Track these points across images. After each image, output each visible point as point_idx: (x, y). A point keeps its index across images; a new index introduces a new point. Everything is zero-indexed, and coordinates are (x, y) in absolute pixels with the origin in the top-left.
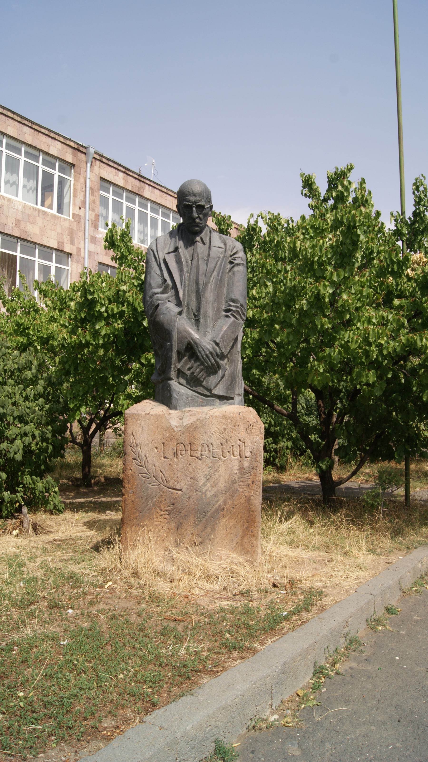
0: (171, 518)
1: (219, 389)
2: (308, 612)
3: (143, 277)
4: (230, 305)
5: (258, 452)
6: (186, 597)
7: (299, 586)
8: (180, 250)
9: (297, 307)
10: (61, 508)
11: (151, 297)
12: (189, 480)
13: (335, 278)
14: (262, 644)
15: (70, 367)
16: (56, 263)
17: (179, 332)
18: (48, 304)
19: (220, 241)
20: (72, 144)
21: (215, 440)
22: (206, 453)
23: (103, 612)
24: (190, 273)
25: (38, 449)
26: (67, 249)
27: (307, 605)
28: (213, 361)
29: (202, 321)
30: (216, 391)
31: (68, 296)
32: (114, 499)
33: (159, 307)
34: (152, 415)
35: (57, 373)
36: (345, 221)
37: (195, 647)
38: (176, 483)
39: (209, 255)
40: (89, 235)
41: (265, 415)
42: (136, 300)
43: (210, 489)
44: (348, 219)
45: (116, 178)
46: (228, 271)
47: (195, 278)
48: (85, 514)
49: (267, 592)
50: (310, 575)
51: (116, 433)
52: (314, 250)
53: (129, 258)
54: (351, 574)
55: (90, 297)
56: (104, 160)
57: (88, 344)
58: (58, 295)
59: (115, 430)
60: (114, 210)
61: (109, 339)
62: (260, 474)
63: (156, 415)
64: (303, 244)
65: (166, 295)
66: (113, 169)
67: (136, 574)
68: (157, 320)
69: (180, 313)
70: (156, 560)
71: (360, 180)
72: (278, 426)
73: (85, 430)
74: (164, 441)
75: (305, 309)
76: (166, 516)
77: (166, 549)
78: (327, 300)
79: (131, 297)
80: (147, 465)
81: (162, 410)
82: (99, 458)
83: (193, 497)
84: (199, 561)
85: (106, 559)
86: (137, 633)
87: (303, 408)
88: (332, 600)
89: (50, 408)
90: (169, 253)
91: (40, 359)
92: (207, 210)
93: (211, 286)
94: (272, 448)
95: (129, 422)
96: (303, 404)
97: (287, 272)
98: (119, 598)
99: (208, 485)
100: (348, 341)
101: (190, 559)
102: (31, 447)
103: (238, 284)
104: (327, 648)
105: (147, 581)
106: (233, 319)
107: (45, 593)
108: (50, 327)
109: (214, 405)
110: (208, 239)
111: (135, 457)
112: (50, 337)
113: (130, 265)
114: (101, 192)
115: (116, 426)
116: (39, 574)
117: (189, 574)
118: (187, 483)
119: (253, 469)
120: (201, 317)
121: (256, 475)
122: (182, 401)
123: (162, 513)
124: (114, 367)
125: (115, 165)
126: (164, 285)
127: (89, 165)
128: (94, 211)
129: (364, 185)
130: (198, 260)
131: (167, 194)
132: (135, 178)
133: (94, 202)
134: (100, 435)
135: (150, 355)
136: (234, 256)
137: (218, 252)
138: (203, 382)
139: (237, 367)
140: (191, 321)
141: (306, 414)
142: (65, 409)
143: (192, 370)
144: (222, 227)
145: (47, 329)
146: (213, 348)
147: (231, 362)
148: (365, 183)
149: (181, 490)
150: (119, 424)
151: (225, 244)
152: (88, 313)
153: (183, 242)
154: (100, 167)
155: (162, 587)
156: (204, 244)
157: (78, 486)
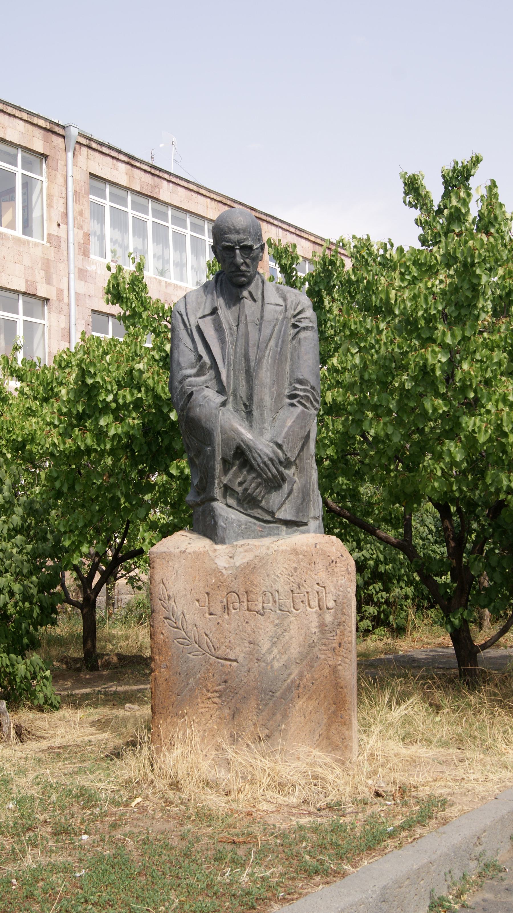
0: (223, 702)
1: (285, 510)
2: (424, 826)
3: (168, 347)
4: (296, 389)
5: (345, 601)
6: (249, 814)
7: (414, 794)
8: (219, 311)
9: (397, 385)
10: (55, 703)
11: (181, 382)
12: (247, 645)
13: (448, 340)
14: (354, 866)
15: (62, 485)
16: (24, 314)
17: (223, 432)
18: (25, 391)
19: (277, 295)
20: (42, 123)
21: (282, 586)
22: (270, 605)
23: (131, 835)
24: (236, 345)
25: (18, 612)
26: (41, 292)
27: (424, 818)
28: (274, 470)
29: (255, 413)
30: (281, 515)
31: (56, 379)
32: (135, 687)
33: (194, 397)
34: (190, 554)
35: (44, 496)
36: (459, 255)
37: (260, 872)
38: (228, 650)
39: (262, 317)
40: (75, 267)
41: (369, 546)
42: (158, 382)
43: (278, 657)
44: (463, 253)
45: (115, 172)
46: (290, 338)
47: (243, 352)
48: (92, 710)
49: (366, 804)
50: (431, 779)
51: (132, 584)
52: (416, 302)
53: (144, 315)
54: (491, 776)
55: (90, 381)
56: (94, 145)
57: (89, 451)
58: (41, 379)
59: (131, 580)
60: (113, 225)
61: (119, 442)
62: (350, 632)
63: (195, 552)
64: (399, 294)
65: (202, 379)
66: (108, 159)
67: (175, 786)
68: (191, 414)
69: (224, 404)
70: (205, 765)
71: (489, 183)
72: (391, 562)
73: (85, 582)
74: (208, 590)
75: (406, 387)
76: (216, 700)
77: (219, 748)
78: (438, 373)
79: (151, 380)
80: (185, 627)
81: (203, 545)
82: (107, 627)
83: (253, 670)
84: (267, 763)
85: (131, 767)
86: (181, 859)
87: (430, 531)
88: (459, 810)
89: (33, 549)
90: (204, 317)
91: (14, 476)
92: (257, 251)
93: (267, 363)
94: (382, 598)
95: (156, 565)
96: (430, 526)
97: (380, 332)
98: (153, 818)
99: (275, 651)
100: (473, 431)
101: (253, 761)
102: (7, 610)
103: (306, 357)
104: (450, 872)
105: (192, 794)
106: (300, 408)
107: (46, 816)
108: (27, 424)
109: (279, 534)
110: (260, 292)
111: (167, 616)
112: (27, 441)
113: (147, 326)
114: (91, 196)
115: (132, 574)
116: (35, 792)
117: (252, 782)
118: (245, 650)
119: (339, 625)
120: (254, 407)
121: (343, 635)
122: (232, 531)
123: (210, 695)
124: (128, 481)
125: (112, 153)
126: (199, 364)
127: (70, 154)
128: (81, 227)
129: (494, 191)
130: (246, 325)
131: (199, 193)
132: (145, 171)
133: (81, 213)
134: (108, 589)
135: (183, 463)
136: (299, 317)
137: (276, 311)
138: (261, 501)
139: (310, 478)
140: (240, 415)
141: (436, 542)
142: (57, 551)
143: (244, 486)
144: (284, 261)
145: (22, 428)
146: (274, 452)
147: (301, 470)
148: (495, 186)
149: (235, 661)
150: (137, 570)
151: (285, 300)
152: (88, 404)
153: (224, 299)
154: (88, 158)
155: (214, 801)
156: (255, 300)
157: (79, 670)
